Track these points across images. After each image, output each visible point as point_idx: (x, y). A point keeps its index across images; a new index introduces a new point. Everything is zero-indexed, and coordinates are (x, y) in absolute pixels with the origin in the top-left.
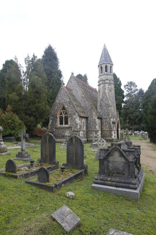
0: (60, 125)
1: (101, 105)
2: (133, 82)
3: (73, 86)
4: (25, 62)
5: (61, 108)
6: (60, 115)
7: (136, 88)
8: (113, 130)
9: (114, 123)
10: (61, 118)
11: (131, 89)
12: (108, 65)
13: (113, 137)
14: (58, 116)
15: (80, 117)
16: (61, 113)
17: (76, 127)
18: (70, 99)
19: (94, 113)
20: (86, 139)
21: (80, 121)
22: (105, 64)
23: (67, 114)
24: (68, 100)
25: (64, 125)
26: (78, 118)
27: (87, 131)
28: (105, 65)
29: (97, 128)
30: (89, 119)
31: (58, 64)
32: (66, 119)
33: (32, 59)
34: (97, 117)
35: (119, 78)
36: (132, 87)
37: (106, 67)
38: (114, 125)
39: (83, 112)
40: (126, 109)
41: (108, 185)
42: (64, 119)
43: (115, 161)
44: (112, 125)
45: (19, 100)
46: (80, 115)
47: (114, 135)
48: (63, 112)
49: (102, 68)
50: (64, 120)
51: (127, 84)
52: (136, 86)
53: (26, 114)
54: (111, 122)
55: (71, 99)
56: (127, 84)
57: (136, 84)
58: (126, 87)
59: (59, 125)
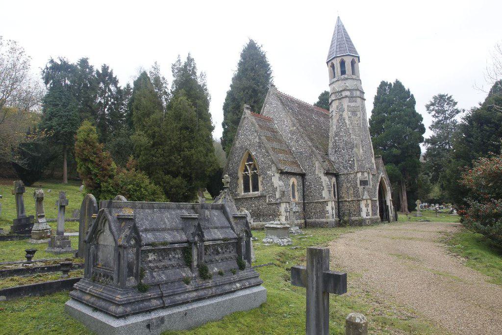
0: (244, 192)
1: (336, 146)
2: (447, 95)
3: (274, 112)
4: (173, 71)
5: (245, 156)
6: (245, 171)
7: (455, 108)
8: (363, 200)
9: (364, 183)
10: (246, 178)
11: (444, 112)
12: (345, 58)
13: (364, 215)
14: (240, 174)
15: (282, 173)
16: (246, 167)
17: (274, 196)
18: (260, 139)
19: (317, 164)
20: (303, 221)
21: (281, 183)
22: (341, 58)
23: (256, 170)
24: (257, 140)
25: (252, 193)
26: (277, 175)
27: (304, 203)
28: (339, 60)
29: (324, 196)
30: (307, 177)
31: (269, 74)
32: (255, 177)
33: (185, 66)
34: (322, 171)
35: (409, 90)
36: (446, 107)
37: (343, 63)
38: (364, 188)
39: (296, 163)
40: (435, 156)
41: (87, 304)
42: (252, 180)
43: (106, 244)
44: (361, 188)
45: (153, 146)
46: (281, 170)
47: (364, 209)
48: (250, 165)
49: (333, 66)
50: (250, 181)
51: (433, 102)
52: (455, 103)
53: (167, 172)
54: (358, 182)
55: (263, 138)
56: (433, 102)
57: (455, 98)
58: (432, 108)
59: (243, 194)
